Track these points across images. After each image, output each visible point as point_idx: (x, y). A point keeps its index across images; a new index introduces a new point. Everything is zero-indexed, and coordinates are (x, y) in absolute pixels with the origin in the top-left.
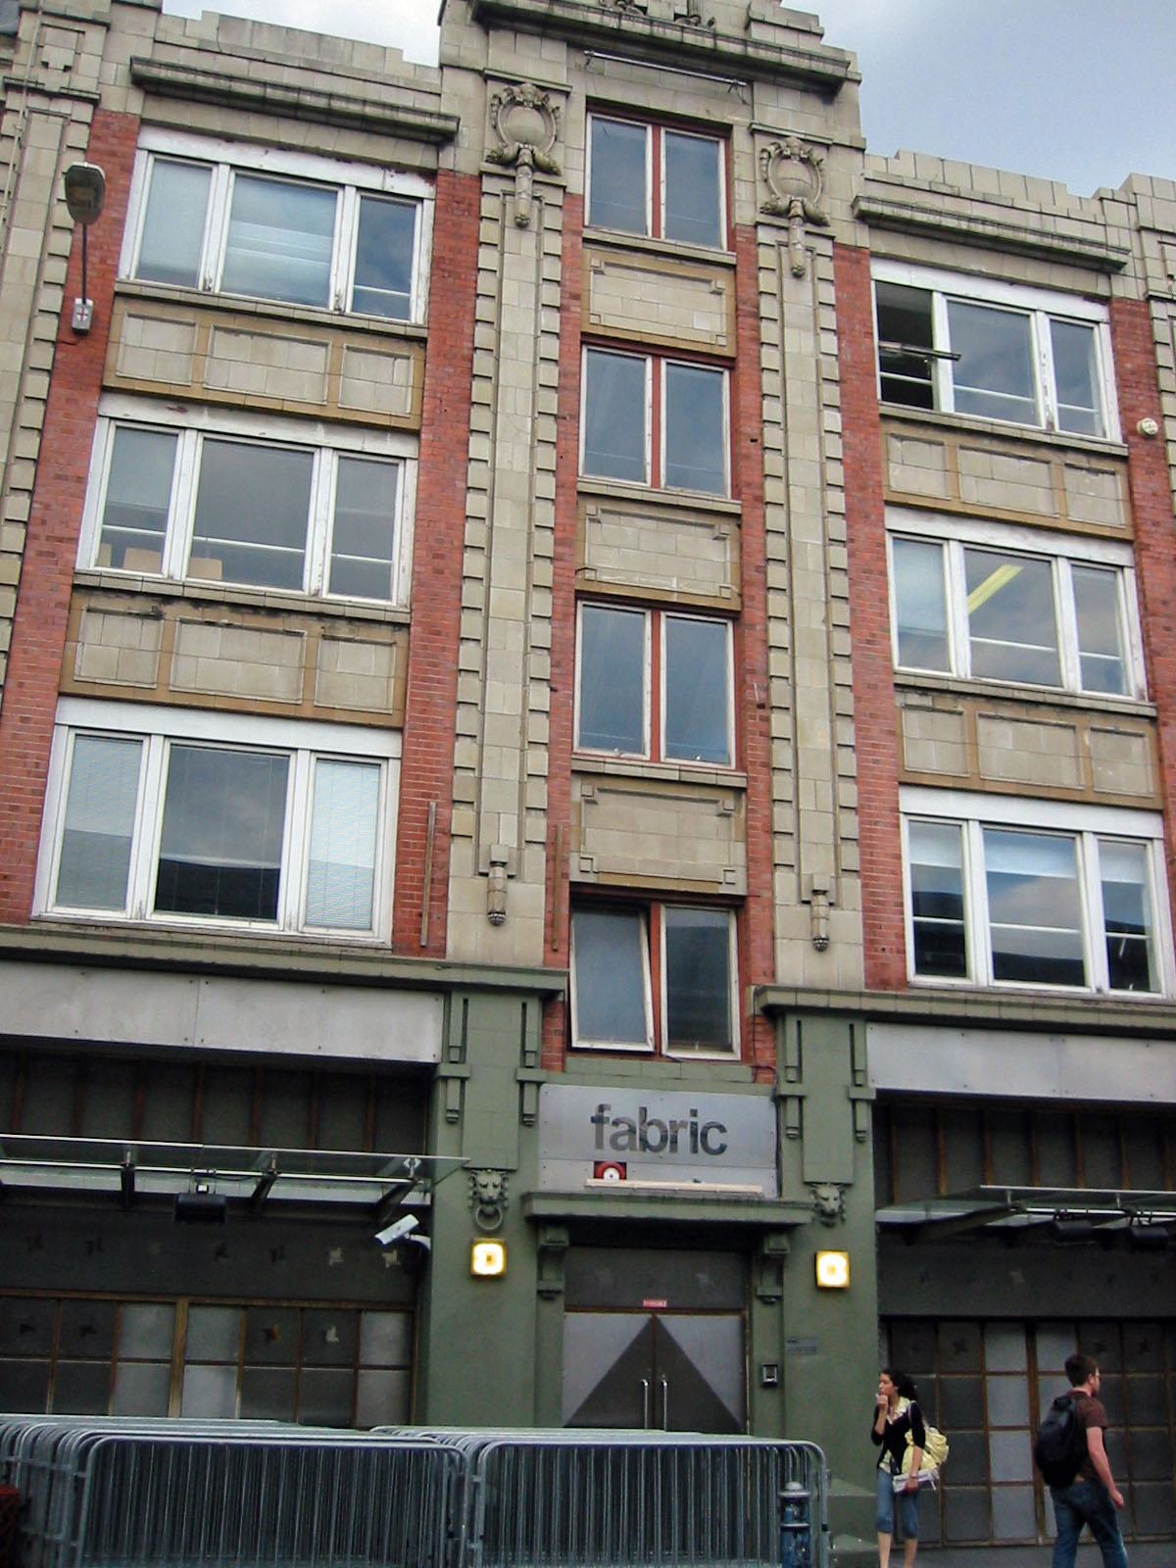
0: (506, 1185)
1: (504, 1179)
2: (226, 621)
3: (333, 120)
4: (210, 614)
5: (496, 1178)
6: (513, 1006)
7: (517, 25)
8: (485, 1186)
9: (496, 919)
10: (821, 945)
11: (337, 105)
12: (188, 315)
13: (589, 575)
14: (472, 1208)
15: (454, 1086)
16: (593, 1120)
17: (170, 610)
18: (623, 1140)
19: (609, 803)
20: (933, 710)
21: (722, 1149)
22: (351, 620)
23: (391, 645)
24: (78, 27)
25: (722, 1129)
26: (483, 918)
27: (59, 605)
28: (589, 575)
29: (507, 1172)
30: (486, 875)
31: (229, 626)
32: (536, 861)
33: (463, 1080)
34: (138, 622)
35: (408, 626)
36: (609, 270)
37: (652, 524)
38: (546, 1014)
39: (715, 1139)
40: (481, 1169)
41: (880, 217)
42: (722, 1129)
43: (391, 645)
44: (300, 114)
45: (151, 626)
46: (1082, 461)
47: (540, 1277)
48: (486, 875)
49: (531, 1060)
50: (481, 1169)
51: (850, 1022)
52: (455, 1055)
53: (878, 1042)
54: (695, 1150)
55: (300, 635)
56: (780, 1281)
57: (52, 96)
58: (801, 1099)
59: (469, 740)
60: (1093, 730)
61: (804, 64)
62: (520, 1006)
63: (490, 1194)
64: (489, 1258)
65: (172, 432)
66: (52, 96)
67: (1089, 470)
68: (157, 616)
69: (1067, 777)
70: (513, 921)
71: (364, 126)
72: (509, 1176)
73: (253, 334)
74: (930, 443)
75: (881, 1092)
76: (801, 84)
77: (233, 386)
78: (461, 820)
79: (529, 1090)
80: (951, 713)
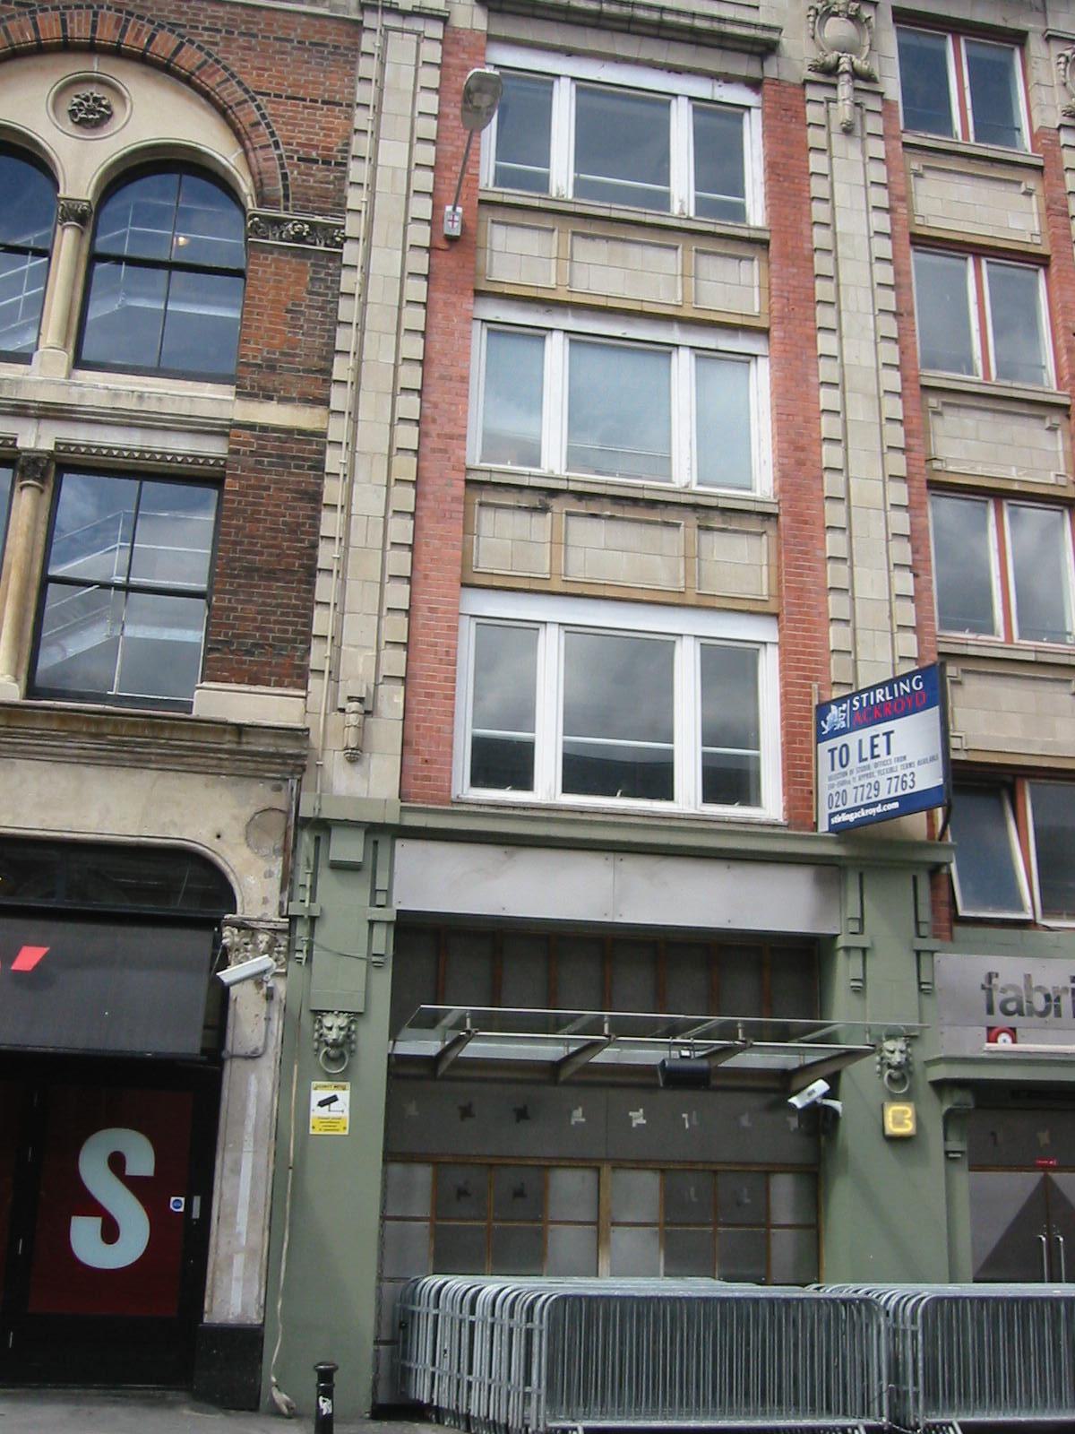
1: (351, 1022)
2: (608, 513)
3: (664, 33)
5: (342, 1021)
12: (548, 222)
13: (936, 465)
14: (881, 1073)
16: (983, 987)
17: (557, 505)
22: (725, 510)
27: (455, 499)
28: (936, 465)
31: (611, 517)
33: (864, 950)
35: (776, 516)
36: (928, 174)
40: (328, 1012)
44: (633, 28)
47: (946, 1139)
50: (328, 1012)
55: (678, 526)
58: (313, 919)
63: (898, 1060)
64: (900, 1119)
65: (539, 335)
68: (544, 510)
71: (694, 38)
75: (399, 912)
79: (925, 958)
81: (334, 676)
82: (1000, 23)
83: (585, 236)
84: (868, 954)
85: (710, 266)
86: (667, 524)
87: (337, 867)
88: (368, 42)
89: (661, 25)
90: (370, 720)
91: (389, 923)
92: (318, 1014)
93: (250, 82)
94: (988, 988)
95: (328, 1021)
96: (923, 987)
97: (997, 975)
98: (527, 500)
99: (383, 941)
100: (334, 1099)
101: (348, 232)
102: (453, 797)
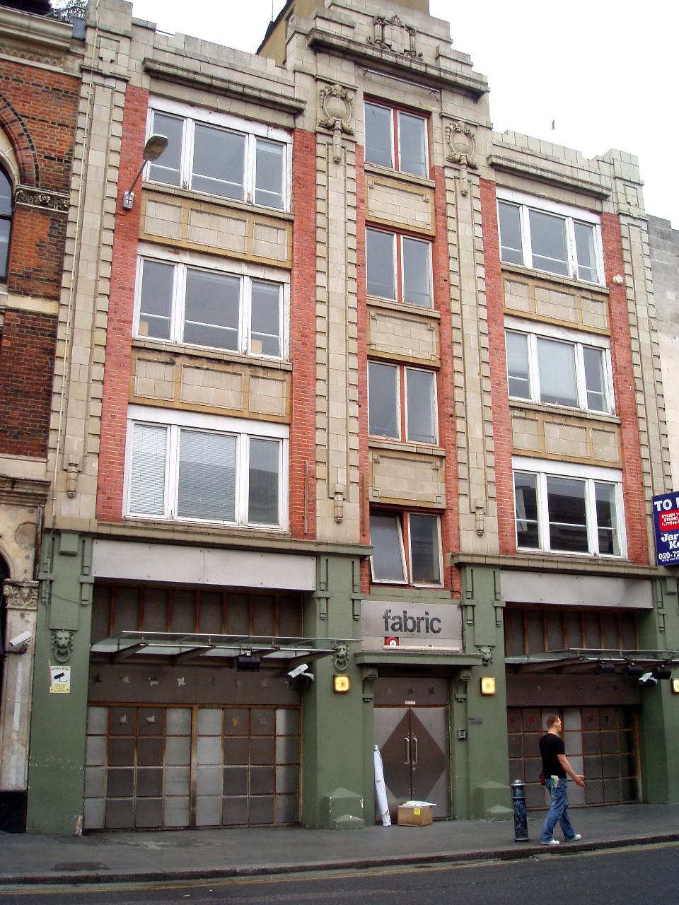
0: (72, 638)
1: (71, 635)
2: (205, 367)
4: (198, 363)
6: (348, 562)
7: (331, 52)
8: (61, 639)
9: (480, 533)
10: (480, 533)
11: (248, 91)
12: (178, 202)
13: (372, 347)
15: (323, 602)
17: (178, 360)
18: (397, 627)
19: (385, 463)
20: (525, 419)
21: (440, 629)
23: (283, 381)
24: (116, 38)
25: (439, 621)
26: (332, 519)
28: (372, 347)
29: (72, 632)
30: (333, 498)
31: (207, 369)
32: (355, 491)
33: (327, 599)
34: (163, 366)
37: (399, 322)
38: (362, 567)
39: (436, 625)
41: (501, 166)
42: (439, 621)
43: (283, 381)
45: (169, 368)
46: (589, 295)
47: (363, 692)
48: (333, 498)
49: (356, 589)
51: (493, 570)
52: (323, 587)
53: (506, 579)
54: (427, 631)
55: (241, 375)
56: (465, 692)
57: (105, 76)
58: (51, 582)
59: (322, 431)
60: (593, 429)
61: (467, 83)
62: (51, 539)
66: (635, 218)
67: (592, 300)
68: (173, 363)
69: (582, 452)
70: (346, 521)
71: (260, 103)
72: (74, 633)
73: (209, 213)
74: (522, 284)
75: (507, 603)
76: (464, 93)
77: (202, 241)
78: (320, 471)
80: (533, 420)
81: (327, 480)
82: (418, 106)
83: (197, 211)
84: (475, 608)
85: (196, 219)
86: (235, 374)
87: (63, 554)
88: (84, 91)
89: (243, 94)
90: (81, 476)
91: (91, 584)
92: (54, 631)
93: (18, 109)
94: (386, 618)
95: (67, 635)
96: (356, 617)
97: (390, 611)
98: (163, 358)
99: (88, 592)
100: (62, 675)
101: (72, 202)
102: (318, 540)
